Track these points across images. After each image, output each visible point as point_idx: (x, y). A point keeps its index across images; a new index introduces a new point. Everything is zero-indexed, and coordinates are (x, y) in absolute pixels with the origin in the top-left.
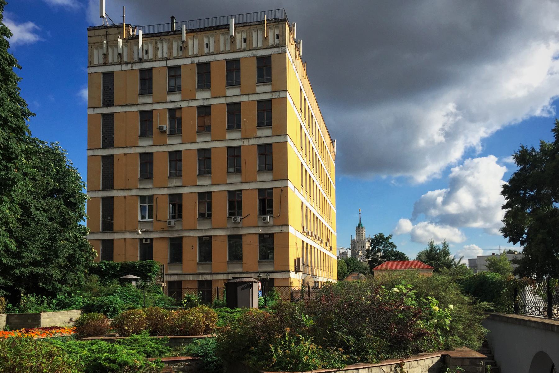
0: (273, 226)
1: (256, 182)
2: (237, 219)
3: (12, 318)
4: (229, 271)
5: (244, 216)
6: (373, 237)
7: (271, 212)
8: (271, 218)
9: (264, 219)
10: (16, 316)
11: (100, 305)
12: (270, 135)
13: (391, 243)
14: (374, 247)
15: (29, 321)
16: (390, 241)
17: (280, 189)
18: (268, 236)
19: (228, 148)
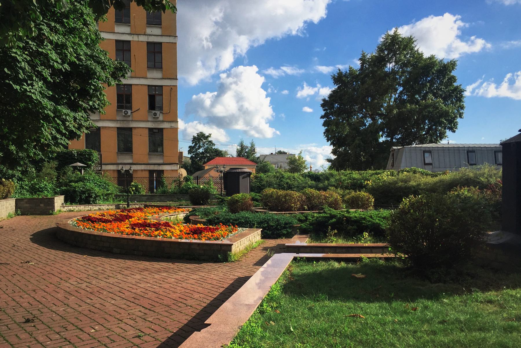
0: (163, 121)
1: (146, 78)
2: (127, 112)
3: (22, 203)
4: (119, 162)
5: (133, 110)
6: (196, 135)
7: (161, 109)
8: (161, 115)
9: (155, 114)
10: (26, 200)
11: (82, 191)
12: (160, 33)
13: (210, 142)
14: (196, 145)
15: (42, 205)
16: (210, 139)
17: (170, 88)
18: (157, 131)
19: (117, 41)
